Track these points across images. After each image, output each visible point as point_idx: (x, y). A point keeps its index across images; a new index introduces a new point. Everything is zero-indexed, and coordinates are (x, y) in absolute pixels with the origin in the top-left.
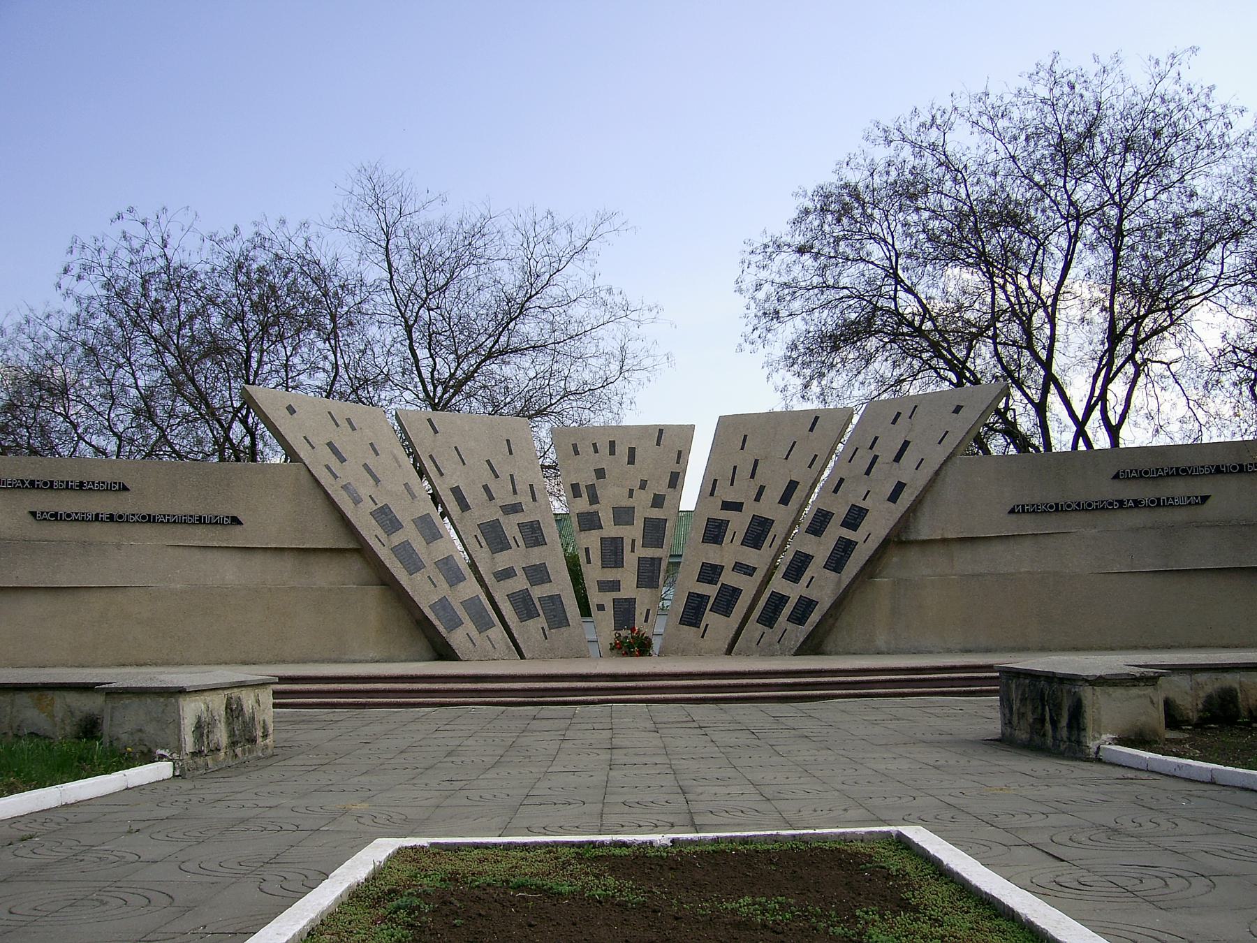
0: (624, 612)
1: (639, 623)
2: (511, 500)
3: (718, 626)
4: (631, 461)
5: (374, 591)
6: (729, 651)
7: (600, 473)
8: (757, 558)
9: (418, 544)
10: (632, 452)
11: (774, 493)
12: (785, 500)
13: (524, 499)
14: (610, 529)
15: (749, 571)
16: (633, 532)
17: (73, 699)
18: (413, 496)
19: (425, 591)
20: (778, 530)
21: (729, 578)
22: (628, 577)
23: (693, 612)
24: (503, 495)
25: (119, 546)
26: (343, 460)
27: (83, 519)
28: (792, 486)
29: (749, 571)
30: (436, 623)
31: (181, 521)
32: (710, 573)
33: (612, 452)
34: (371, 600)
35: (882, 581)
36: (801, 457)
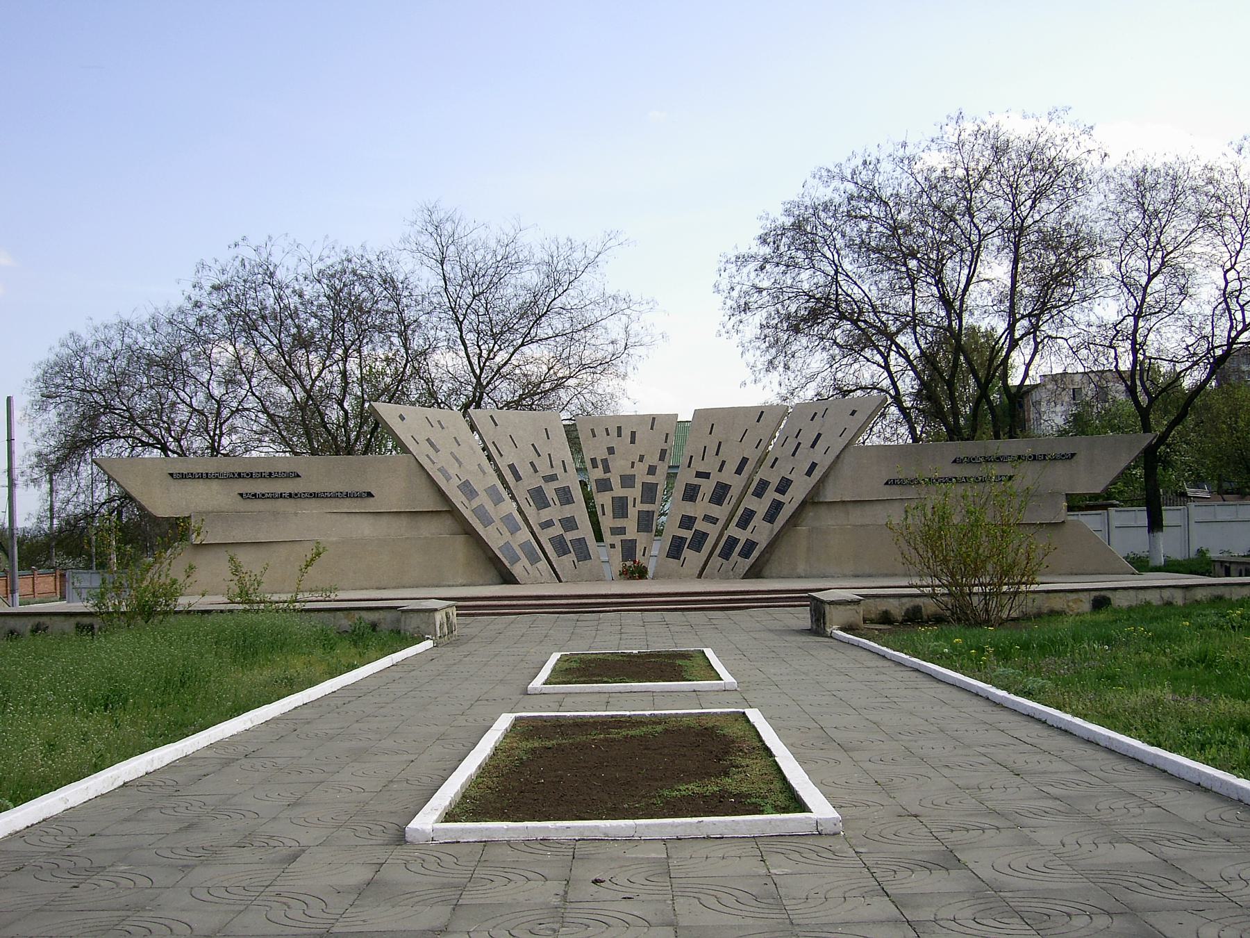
0: (629, 549)
1: (638, 556)
2: (550, 472)
3: (693, 558)
4: (633, 442)
5: (461, 539)
6: (700, 576)
7: (611, 451)
8: (720, 512)
9: (489, 506)
10: (633, 434)
11: (731, 466)
12: (739, 471)
13: (558, 471)
14: (618, 491)
15: (714, 521)
16: (635, 493)
17: (364, 614)
18: (484, 473)
19: (495, 538)
20: (734, 492)
21: (700, 526)
22: (631, 524)
23: (676, 549)
24: (544, 469)
25: (296, 514)
26: (437, 451)
27: (273, 497)
28: (744, 461)
29: (714, 521)
30: (503, 559)
31: (335, 496)
32: (687, 522)
33: (619, 435)
34: (459, 545)
35: (802, 529)
36: (751, 439)
